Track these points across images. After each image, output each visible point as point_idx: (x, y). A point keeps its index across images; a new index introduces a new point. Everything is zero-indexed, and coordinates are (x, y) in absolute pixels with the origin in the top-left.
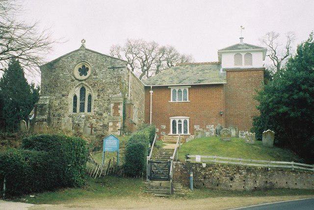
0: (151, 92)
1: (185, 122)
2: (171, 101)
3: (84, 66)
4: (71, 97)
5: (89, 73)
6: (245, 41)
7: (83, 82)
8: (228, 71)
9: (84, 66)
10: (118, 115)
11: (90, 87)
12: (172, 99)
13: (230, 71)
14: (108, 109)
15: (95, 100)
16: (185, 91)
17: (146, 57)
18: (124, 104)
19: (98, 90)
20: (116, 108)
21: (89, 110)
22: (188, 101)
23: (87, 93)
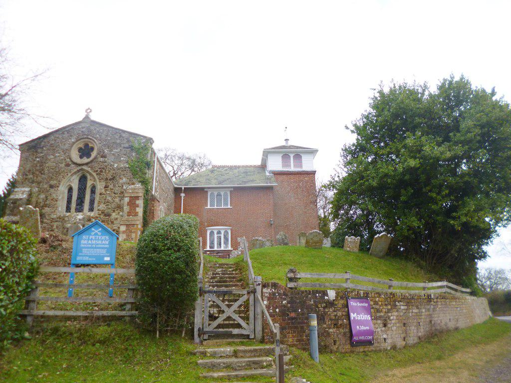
0: (183, 195)
1: (226, 232)
2: (209, 207)
3: (86, 145)
4: (63, 189)
5: (94, 154)
6: (290, 143)
7: (85, 167)
8: (277, 174)
9: (86, 145)
10: (136, 214)
11: (94, 174)
12: (209, 204)
14: (120, 207)
15: (101, 194)
16: (226, 194)
17: (174, 172)
19: (107, 179)
20: (132, 204)
22: (229, 207)
23: (89, 184)
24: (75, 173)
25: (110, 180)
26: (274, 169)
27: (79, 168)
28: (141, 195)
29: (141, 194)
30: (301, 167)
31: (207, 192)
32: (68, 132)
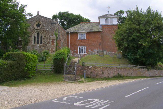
0: (69, 35)
3: (38, 23)
4: (33, 37)
5: (41, 26)
6: (110, 13)
7: (38, 30)
8: (103, 26)
9: (38, 23)
10: (54, 45)
11: (41, 32)
13: (104, 26)
14: (49, 42)
18: (56, 41)
21: (41, 43)
24: (36, 32)
27: (37, 31)
28: (55, 39)
29: (55, 38)
30: (113, 23)
31: (78, 34)
32: (33, 19)
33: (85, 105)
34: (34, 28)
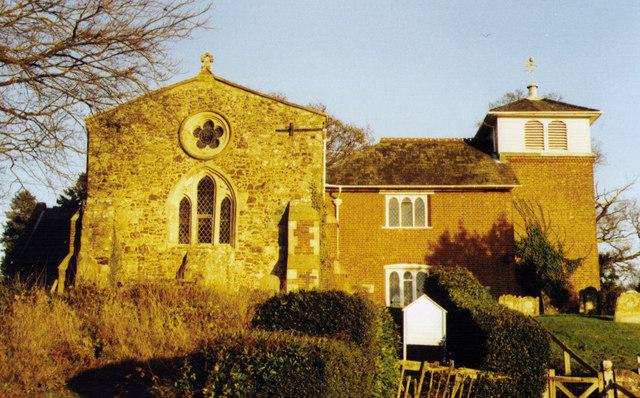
3: (221, 131)
4: (174, 201)
10: (310, 252)
11: (228, 177)
19: (251, 187)
23: (221, 194)
25: (257, 188)
26: (512, 151)
30: (566, 148)
33: (505, 110)
34: (187, 153)
